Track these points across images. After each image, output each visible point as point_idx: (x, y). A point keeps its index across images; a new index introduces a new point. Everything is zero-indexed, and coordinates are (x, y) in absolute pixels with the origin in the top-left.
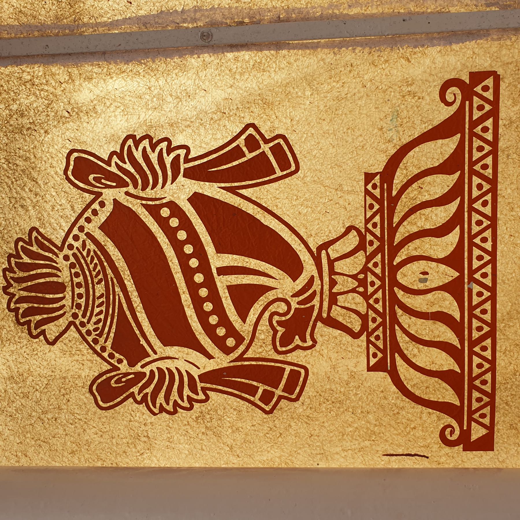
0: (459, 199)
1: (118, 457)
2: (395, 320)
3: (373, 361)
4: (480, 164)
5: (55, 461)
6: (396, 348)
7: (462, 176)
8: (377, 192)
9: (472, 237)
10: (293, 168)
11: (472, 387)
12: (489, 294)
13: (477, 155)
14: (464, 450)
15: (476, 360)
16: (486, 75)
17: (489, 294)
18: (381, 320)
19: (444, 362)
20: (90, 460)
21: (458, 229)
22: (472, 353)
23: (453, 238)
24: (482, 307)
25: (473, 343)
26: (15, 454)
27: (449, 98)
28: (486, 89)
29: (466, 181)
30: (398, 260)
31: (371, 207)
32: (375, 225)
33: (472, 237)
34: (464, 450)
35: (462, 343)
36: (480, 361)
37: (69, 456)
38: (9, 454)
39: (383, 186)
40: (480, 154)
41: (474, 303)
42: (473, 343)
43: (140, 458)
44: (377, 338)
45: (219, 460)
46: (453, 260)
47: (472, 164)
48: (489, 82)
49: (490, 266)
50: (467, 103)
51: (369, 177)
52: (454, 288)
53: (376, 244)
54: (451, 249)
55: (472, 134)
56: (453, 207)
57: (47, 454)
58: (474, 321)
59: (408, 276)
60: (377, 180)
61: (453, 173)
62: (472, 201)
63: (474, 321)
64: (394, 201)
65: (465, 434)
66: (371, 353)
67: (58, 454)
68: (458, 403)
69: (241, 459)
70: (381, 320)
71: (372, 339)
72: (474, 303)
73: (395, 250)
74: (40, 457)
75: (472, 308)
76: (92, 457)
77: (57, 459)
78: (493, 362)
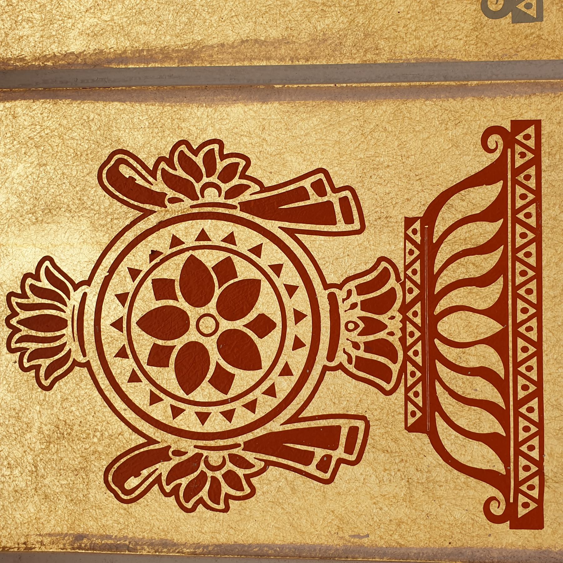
0: (502, 247)
2: (435, 376)
3: (411, 421)
4: (524, 288)
6: (436, 406)
7: (505, 187)
8: (418, 238)
9: (516, 288)
10: (321, 176)
11: (518, 453)
12: (535, 311)
13: (519, 203)
14: (511, 527)
15: (522, 423)
16: (527, 124)
17: (535, 311)
19: (489, 424)
21: (501, 279)
22: (517, 414)
23: (496, 288)
27: (491, 145)
28: (527, 137)
29: (510, 229)
30: (438, 310)
31: (411, 252)
32: (414, 272)
33: (516, 288)
34: (511, 527)
36: (523, 191)
39: (424, 233)
40: (525, 355)
42: (519, 403)
44: (416, 394)
46: (497, 312)
47: (515, 212)
48: (531, 130)
49: (535, 359)
50: (509, 150)
51: (409, 222)
52: (497, 342)
55: (515, 182)
56: (496, 255)
58: (518, 264)
60: (417, 225)
62: (516, 250)
63: (518, 264)
64: (435, 248)
65: (511, 508)
66: (409, 412)
71: (411, 394)
75: (517, 364)
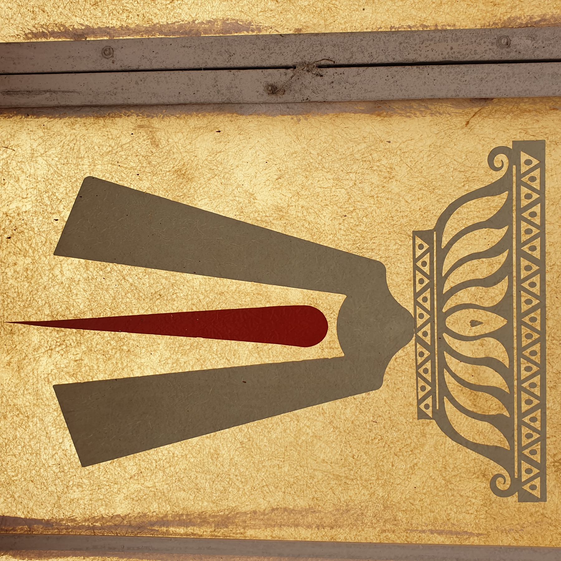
1: (146, 7)
2: (444, 365)
5: (76, 16)
6: (445, 392)
9: (520, 281)
18: (430, 388)
20: (115, 12)
24: (531, 280)
25: (522, 415)
26: (32, 10)
27: (497, 165)
31: (423, 388)
35: (511, 387)
37: (92, 8)
38: (25, 9)
41: (524, 344)
43: (169, 6)
45: (256, 6)
47: (520, 244)
53: (427, 316)
54: (499, 298)
57: (68, 7)
59: (458, 323)
61: (499, 228)
67: (79, 7)
68: (506, 445)
69: (280, 4)
70: (430, 388)
72: (524, 344)
73: (443, 298)
74: (59, 12)
76: (117, 8)
77: (78, 13)
78: (543, 433)
